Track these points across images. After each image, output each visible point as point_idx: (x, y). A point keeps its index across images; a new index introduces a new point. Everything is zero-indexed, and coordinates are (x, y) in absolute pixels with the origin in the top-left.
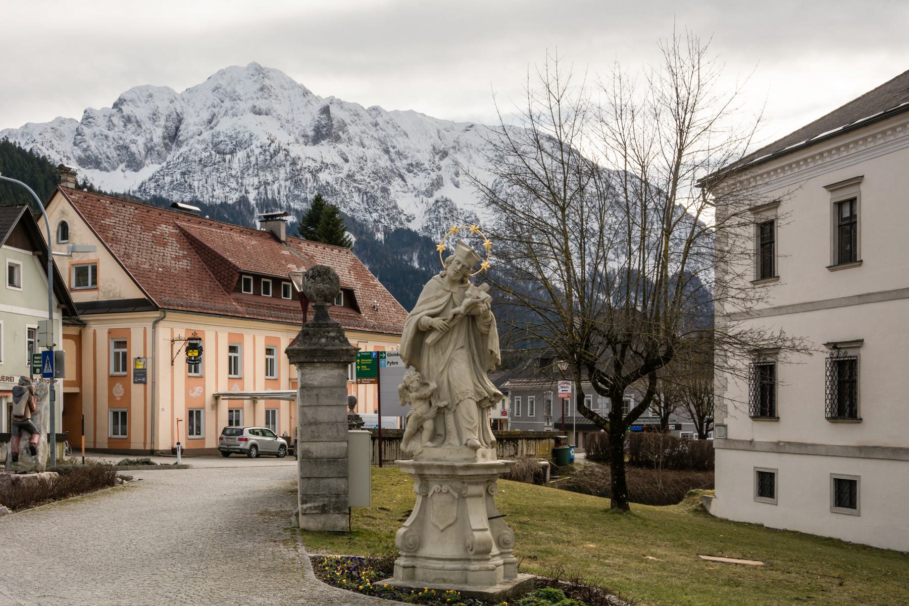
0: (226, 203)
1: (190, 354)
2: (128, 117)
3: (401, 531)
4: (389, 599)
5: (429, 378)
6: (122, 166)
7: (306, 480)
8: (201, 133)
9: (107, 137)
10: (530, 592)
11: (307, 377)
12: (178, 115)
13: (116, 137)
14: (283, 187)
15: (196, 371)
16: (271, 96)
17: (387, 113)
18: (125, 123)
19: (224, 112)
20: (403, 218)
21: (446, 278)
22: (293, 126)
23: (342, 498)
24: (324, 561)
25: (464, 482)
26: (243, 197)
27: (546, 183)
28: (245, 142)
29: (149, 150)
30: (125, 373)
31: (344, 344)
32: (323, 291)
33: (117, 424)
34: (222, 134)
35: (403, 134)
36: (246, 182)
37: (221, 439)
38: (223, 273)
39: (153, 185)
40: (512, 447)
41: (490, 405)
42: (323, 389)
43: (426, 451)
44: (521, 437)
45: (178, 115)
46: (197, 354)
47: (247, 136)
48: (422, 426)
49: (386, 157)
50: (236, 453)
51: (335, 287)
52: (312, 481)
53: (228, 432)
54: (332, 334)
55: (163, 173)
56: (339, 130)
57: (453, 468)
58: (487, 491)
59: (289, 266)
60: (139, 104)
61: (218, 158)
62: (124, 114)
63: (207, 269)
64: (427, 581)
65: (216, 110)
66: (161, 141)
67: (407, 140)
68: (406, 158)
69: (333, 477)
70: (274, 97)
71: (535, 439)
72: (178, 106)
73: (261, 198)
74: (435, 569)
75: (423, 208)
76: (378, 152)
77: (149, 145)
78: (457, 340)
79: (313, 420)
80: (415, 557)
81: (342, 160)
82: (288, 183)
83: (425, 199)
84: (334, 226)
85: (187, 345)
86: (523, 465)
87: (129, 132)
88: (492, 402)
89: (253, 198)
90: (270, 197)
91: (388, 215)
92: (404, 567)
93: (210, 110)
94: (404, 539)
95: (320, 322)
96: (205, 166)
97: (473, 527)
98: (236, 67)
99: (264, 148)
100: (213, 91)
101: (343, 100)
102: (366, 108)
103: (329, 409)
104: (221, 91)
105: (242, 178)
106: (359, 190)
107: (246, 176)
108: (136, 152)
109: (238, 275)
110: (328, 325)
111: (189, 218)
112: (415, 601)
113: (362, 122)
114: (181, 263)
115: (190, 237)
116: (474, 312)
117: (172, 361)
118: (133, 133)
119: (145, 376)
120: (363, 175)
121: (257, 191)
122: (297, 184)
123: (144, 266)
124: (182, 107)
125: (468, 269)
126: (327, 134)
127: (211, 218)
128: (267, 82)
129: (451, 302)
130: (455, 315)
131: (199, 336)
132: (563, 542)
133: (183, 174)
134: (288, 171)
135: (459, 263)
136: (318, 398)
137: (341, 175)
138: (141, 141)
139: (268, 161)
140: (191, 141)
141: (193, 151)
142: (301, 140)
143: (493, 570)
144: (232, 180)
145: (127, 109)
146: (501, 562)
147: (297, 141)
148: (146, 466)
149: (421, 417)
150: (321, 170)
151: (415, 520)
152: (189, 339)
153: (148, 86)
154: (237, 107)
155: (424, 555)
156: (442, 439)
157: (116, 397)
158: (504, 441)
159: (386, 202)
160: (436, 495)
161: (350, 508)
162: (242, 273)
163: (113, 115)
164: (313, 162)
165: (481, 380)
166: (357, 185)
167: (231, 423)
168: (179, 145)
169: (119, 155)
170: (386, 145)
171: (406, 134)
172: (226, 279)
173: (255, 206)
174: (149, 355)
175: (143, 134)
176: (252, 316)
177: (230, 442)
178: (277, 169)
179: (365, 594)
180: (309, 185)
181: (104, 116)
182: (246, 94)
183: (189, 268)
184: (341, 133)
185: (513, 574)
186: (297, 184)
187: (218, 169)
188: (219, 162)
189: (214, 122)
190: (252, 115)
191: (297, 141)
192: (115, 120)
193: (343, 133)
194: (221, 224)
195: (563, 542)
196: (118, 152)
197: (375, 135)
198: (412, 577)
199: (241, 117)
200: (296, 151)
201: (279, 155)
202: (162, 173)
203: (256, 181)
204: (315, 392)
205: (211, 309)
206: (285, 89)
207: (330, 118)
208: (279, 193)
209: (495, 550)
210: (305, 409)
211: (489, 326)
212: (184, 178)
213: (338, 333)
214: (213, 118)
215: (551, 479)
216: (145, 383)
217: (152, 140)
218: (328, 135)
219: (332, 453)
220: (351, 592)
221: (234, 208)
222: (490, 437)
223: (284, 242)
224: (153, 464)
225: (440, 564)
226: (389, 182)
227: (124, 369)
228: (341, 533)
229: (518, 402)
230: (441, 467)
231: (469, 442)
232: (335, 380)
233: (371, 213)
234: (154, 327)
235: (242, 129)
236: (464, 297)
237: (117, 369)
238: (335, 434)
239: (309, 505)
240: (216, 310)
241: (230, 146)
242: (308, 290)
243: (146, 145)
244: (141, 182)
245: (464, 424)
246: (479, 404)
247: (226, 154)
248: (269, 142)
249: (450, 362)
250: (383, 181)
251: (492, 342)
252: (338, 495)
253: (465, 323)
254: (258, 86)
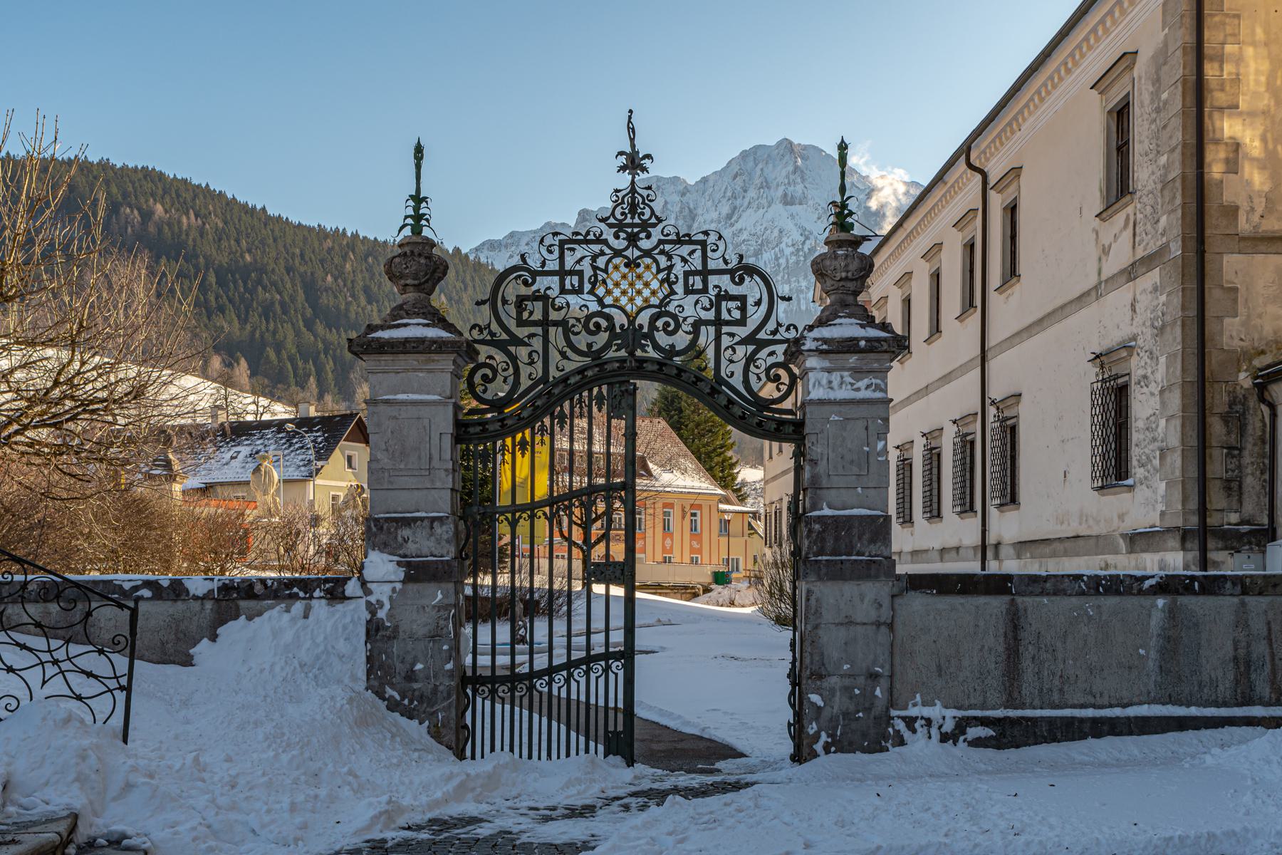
189: (735, 218)
248: (802, 239)
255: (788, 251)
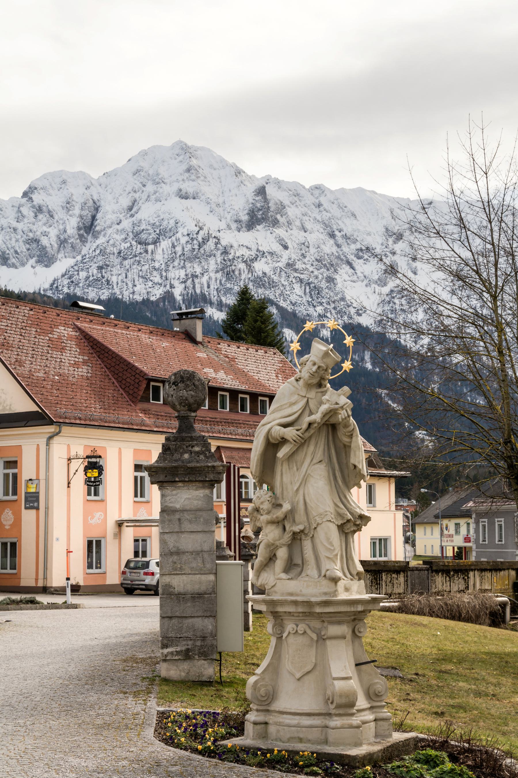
0: (148, 299)
1: (89, 475)
2: (39, 207)
3: (252, 679)
4: (231, 762)
5: (283, 498)
6: (32, 261)
7: (166, 619)
8: (120, 222)
9: (15, 230)
10: (407, 754)
11: (168, 498)
12: (94, 203)
13: (25, 229)
14: (214, 280)
15: (96, 494)
16: (198, 177)
17: (332, 192)
18: (36, 213)
19: (146, 197)
20: (353, 311)
21: (301, 382)
22: (224, 210)
23: (209, 639)
24: (170, 716)
25: (323, 621)
26: (168, 292)
27: (475, 268)
28: (170, 230)
29: (62, 242)
30: (15, 498)
31: (210, 460)
32: (186, 400)
33: (6, 557)
34: (143, 222)
35: (350, 215)
36: (171, 275)
37: (124, 573)
38: (128, 380)
39: (66, 282)
40: (461, 581)
41: (355, 528)
42: (185, 512)
43: (279, 584)
44: (473, 567)
45: (94, 203)
46: (96, 474)
47: (172, 223)
48: (275, 555)
49: (332, 241)
50: (142, 589)
51: (200, 394)
52: (175, 621)
53: (132, 565)
54: (197, 449)
55: (77, 268)
56: (277, 214)
57: (309, 604)
58: (353, 631)
59: (205, 370)
60: (51, 191)
61: (139, 249)
62: (35, 203)
63: (111, 376)
64: (281, 740)
65: (137, 196)
66: (76, 232)
67: (355, 222)
68: (355, 241)
69: (198, 617)
70: (202, 178)
71: (490, 570)
72: (95, 193)
73: (188, 293)
74: (289, 726)
75: (376, 299)
76: (322, 237)
77: (62, 237)
78: (314, 453)
79: (174, 550)
80: (268, 711)
81: (281, 247)
82: (219, 275)
83: (378, 289)
84: (263, 323)
85: (86, 464)
86: (476, 603)
87: (40, 223)
88: (358, 525)
89: (179, 293)
90: (198, 291)
91: (335, 308)
92: (255, 723)
93: (131, 195)
94: (255, 689)
95: (184, 435)
96: (125, 259)
97: (335, 675)
98: (159, 147)
99: (191, 236)
100: (134, 174)
101: (280, 178)
102: (307, 187)
103: (193, 536)
104: (142, 174)
105: (166, 271)
106: (301, 281)
107: (170, 268)
108: (48, 245)
109: (145, 382)
110: (192, 439)
111: (91, 318)
112: (260, 765)
113: (303, 203)
114: (80, 370)
115: (91, 340)
116: (333, 421)
117: (69, 483)
118: (45, 224)
119: (37, 500)
120: (304, 263)
121: (183, 285)
122: (229, 275)
123: (38, 374)
124: (99, 193)
125: (326, 370)
126: (263, 218)
127: (117, 318)
128: (194, 162)
129: (307, 409)
130: (310, 424)
131: (99, 453)
132: (487, 695)
133: (100, 268)
134: (219, 262)
135: (314, 364)
136: (180, 524)
137: (280, 264)
138: (53, 232)
139: (196, 250)
140: (109, 231)
141: (111, 242)
142: (234, 226)
143: (358, 727)
144: (155, 273)
145: (38, 198)
146: (371, 717)
147: (229, 227)
148: (30, 605)
149: (273, 544)
150: (256, 259)
151: (268, 666)
152: (88, 457)
153: (62, 171)
154: (161, 191)
155: (277, 709)
156: (299, 569)
157: (4, 525)
158: (452, 573)
159: (332, 294)
160: (291, 636)
161: (220, 653)
162: (150, 380)
163: (23, 205)
164: (247, 250)
165: (343, 499)
166: (299, 275)
167: (136, 554)
168: (96, 236)
169: (28, 250)
170: (331, 228)
171: (354, 215)
172: (131, 387)
173: (181, 302)
174: (42, 476)
175: (56, 225)
176: (161, 430)
177: (134, 576)
178: (206, 260)
179: (204, 755)
180: (243, 277)
181: (13, 206)
182: (171, 176)
183: (89, 375)
184: (278, 217)
185: (387, 733)
186: (229, 275)
187: (139, 262)
188: (141, 253)
189: (135, 209)
190: (177, 199)
191: (229, 227)
192: (25, 210)
193: (282, 216)
194: (128, 325)
195: (487, 695)
196: (28, 246)
197: (319, 218)
198: (264, 736)
199: (165, 202)
200: (227, 238)
201: (208, 243)
202: (76, 268)
203: (182, 273)
204: (177, 516)
205: (114, 422)
206: (215, 169)
207: (266, 200)
208: (209, 287)
209: (362, 702)
210: (166, 536)
211: (351, 436)
212: (101, 273)
213: (203, 447)
214: (133, 204)
215: (512, 619)
216: (37, 508)
217: (65, 231)
218: (264, 219)
219: (196, 588)
220: (187, 753)
221: (158, 305)
222: (355, 567)
223: (201, 343)
224: (38, 603)
225: (294, 720)
226: (336, 271)
227: (15, 493)
228: (208, 683)
229: (484, 526)
230: (295, 603)
231: (328, 573)
232: (200, 502)
233: (314, 307)
234: (48, 444)
235: (166, 216)
236: (321, 403)
237: (6, 493)
238: (200, 565)
239: (170, 650)
240: (119, 423)
241: (154, 236)
242: (170, 399)
243: (58, 237)
244: (53, 279)
245: (323, 553)
246: (341, 528)
247: (149, 244)
248: (197, 229)
249: (305, 480)
250: (328, 270)
251: (355, 455)
252: (204, 638)
253: (324, 434)
254: (184, 167)
255: (183, 240)
